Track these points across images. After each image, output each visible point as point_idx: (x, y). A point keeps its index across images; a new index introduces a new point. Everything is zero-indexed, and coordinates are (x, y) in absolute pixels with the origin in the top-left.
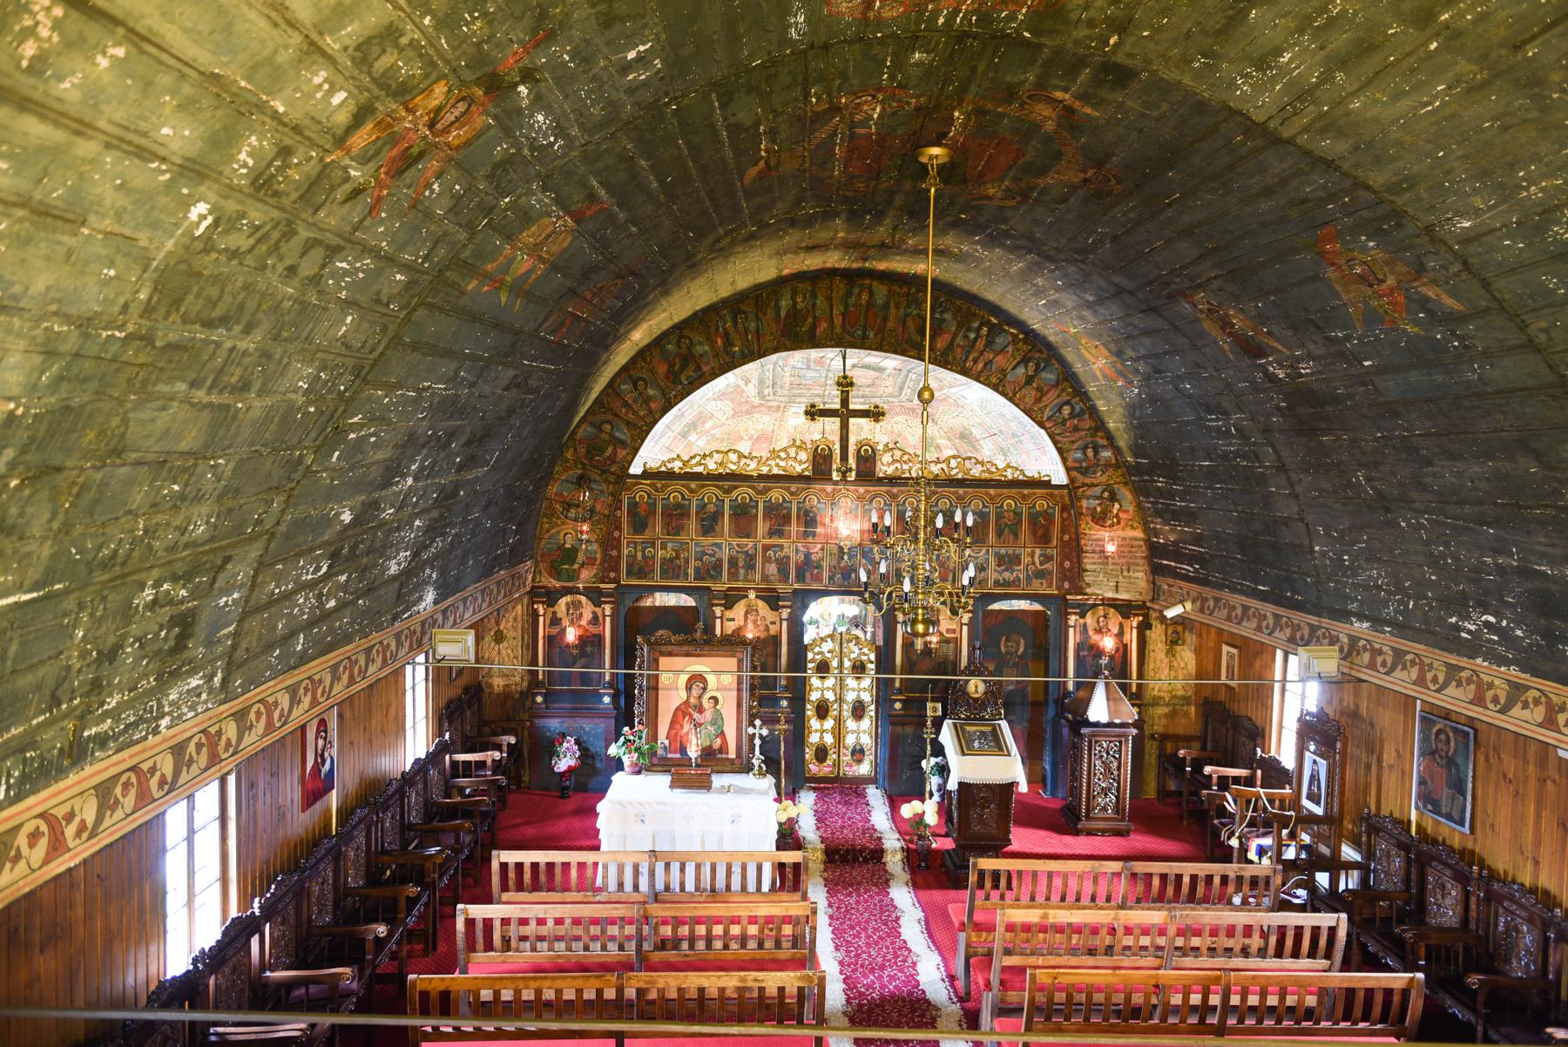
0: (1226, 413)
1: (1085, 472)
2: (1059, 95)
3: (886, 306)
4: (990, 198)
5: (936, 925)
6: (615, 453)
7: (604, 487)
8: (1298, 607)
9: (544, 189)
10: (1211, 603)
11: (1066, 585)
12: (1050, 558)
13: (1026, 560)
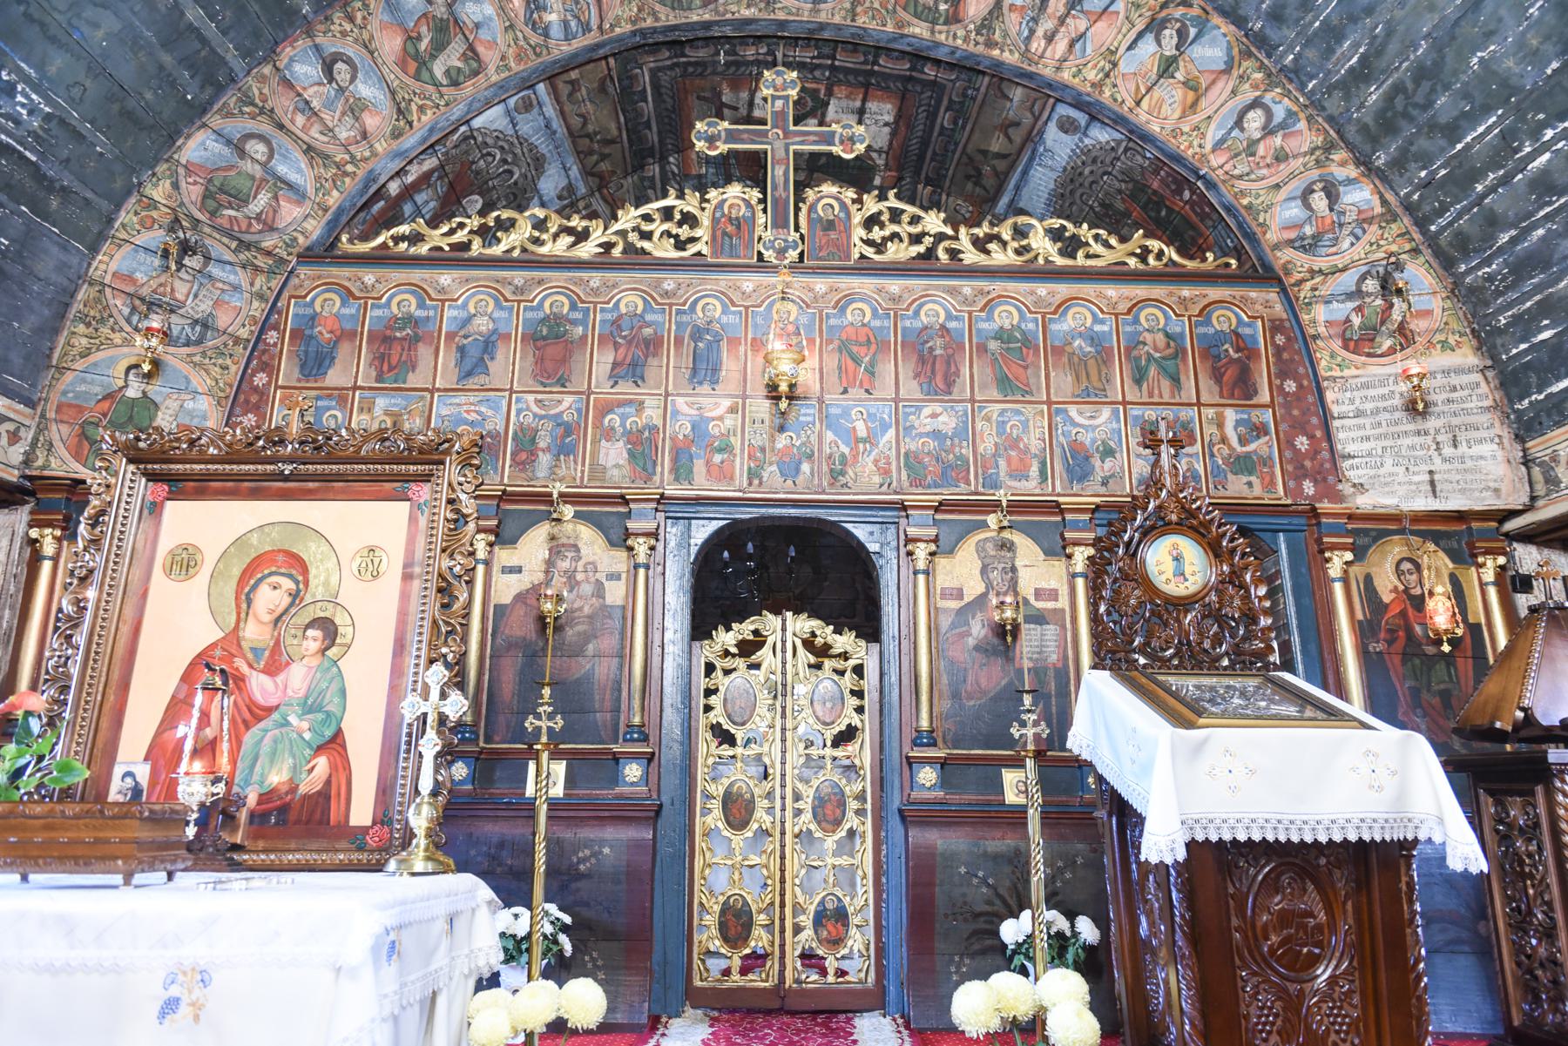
5: (639, 519)
7: (242, 277)
12: (1261, 430)
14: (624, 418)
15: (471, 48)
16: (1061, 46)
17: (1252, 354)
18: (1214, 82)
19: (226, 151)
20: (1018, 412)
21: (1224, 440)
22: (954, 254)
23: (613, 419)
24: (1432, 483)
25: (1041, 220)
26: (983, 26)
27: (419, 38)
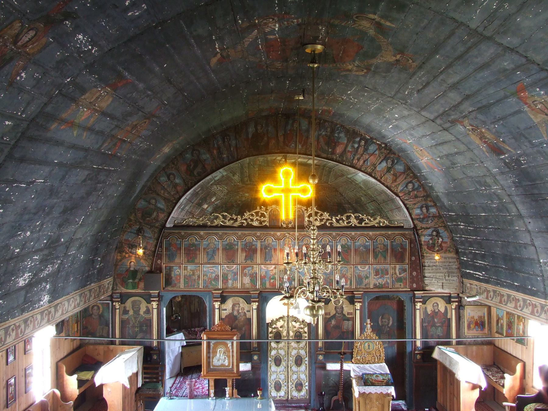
0: (490, 186)
1: (421, 220)
2: (372, 16)
3: (308, 131)
4: (350, 71)
6: (158, 216)
8: (533, 294)
9: (91, 73)
10: (492, 293)
11: (415, 286)
13: (391, 271)
14: (249, 270)
15: (204, 166)
16: (361, 162)
17: (405, 249)
18: (400, 175)
19: (146, 203)
20: (346, 267)
21: (395, 273)
22: (331, 223)
23: (246, 271)
24: (443, 285)
25: (354, 214)
26: (341, 156)
27: (191, 165)
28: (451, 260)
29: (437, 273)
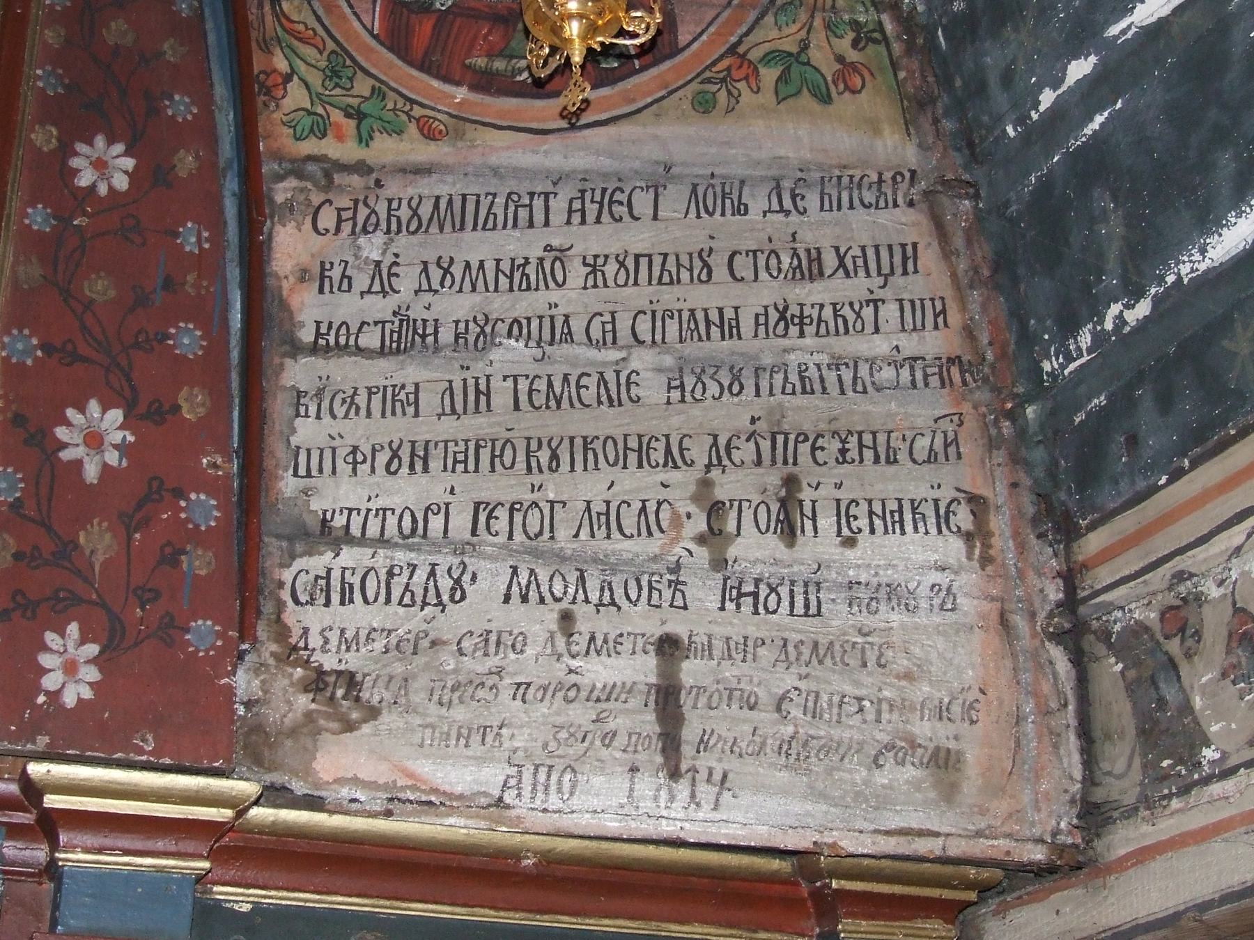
24: (668, 700)
28: (819, 229)
29: (550, 455)
